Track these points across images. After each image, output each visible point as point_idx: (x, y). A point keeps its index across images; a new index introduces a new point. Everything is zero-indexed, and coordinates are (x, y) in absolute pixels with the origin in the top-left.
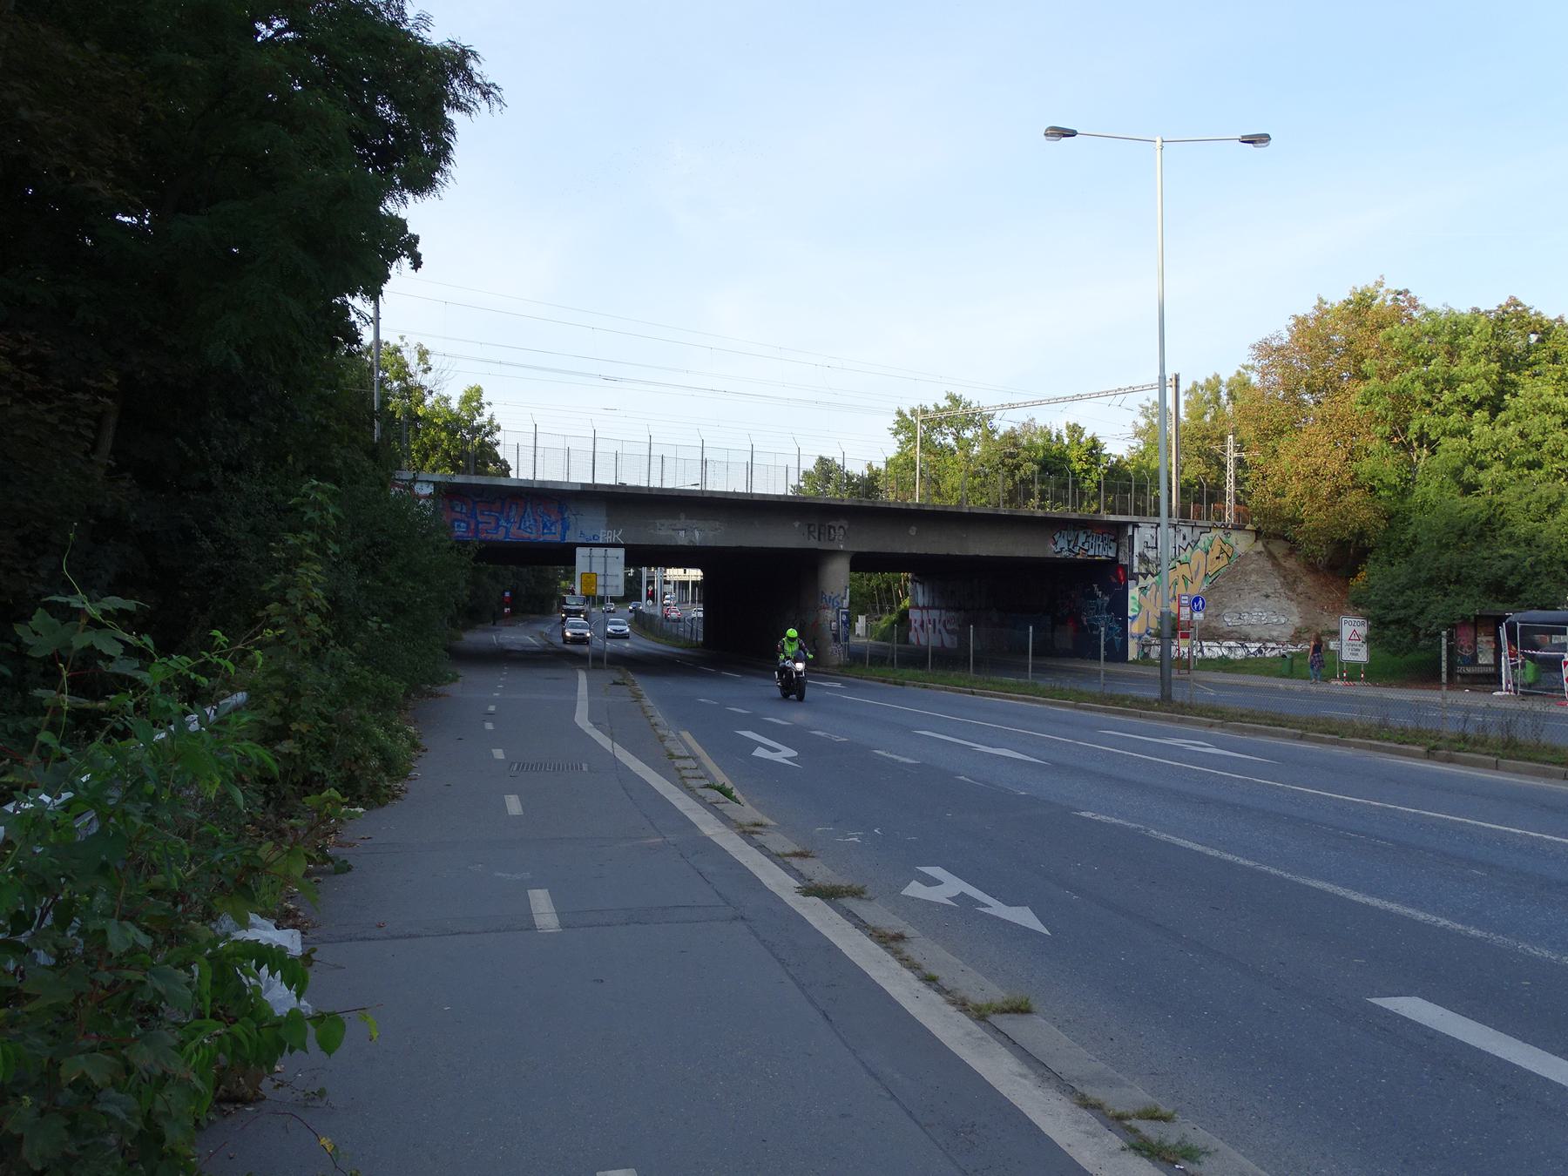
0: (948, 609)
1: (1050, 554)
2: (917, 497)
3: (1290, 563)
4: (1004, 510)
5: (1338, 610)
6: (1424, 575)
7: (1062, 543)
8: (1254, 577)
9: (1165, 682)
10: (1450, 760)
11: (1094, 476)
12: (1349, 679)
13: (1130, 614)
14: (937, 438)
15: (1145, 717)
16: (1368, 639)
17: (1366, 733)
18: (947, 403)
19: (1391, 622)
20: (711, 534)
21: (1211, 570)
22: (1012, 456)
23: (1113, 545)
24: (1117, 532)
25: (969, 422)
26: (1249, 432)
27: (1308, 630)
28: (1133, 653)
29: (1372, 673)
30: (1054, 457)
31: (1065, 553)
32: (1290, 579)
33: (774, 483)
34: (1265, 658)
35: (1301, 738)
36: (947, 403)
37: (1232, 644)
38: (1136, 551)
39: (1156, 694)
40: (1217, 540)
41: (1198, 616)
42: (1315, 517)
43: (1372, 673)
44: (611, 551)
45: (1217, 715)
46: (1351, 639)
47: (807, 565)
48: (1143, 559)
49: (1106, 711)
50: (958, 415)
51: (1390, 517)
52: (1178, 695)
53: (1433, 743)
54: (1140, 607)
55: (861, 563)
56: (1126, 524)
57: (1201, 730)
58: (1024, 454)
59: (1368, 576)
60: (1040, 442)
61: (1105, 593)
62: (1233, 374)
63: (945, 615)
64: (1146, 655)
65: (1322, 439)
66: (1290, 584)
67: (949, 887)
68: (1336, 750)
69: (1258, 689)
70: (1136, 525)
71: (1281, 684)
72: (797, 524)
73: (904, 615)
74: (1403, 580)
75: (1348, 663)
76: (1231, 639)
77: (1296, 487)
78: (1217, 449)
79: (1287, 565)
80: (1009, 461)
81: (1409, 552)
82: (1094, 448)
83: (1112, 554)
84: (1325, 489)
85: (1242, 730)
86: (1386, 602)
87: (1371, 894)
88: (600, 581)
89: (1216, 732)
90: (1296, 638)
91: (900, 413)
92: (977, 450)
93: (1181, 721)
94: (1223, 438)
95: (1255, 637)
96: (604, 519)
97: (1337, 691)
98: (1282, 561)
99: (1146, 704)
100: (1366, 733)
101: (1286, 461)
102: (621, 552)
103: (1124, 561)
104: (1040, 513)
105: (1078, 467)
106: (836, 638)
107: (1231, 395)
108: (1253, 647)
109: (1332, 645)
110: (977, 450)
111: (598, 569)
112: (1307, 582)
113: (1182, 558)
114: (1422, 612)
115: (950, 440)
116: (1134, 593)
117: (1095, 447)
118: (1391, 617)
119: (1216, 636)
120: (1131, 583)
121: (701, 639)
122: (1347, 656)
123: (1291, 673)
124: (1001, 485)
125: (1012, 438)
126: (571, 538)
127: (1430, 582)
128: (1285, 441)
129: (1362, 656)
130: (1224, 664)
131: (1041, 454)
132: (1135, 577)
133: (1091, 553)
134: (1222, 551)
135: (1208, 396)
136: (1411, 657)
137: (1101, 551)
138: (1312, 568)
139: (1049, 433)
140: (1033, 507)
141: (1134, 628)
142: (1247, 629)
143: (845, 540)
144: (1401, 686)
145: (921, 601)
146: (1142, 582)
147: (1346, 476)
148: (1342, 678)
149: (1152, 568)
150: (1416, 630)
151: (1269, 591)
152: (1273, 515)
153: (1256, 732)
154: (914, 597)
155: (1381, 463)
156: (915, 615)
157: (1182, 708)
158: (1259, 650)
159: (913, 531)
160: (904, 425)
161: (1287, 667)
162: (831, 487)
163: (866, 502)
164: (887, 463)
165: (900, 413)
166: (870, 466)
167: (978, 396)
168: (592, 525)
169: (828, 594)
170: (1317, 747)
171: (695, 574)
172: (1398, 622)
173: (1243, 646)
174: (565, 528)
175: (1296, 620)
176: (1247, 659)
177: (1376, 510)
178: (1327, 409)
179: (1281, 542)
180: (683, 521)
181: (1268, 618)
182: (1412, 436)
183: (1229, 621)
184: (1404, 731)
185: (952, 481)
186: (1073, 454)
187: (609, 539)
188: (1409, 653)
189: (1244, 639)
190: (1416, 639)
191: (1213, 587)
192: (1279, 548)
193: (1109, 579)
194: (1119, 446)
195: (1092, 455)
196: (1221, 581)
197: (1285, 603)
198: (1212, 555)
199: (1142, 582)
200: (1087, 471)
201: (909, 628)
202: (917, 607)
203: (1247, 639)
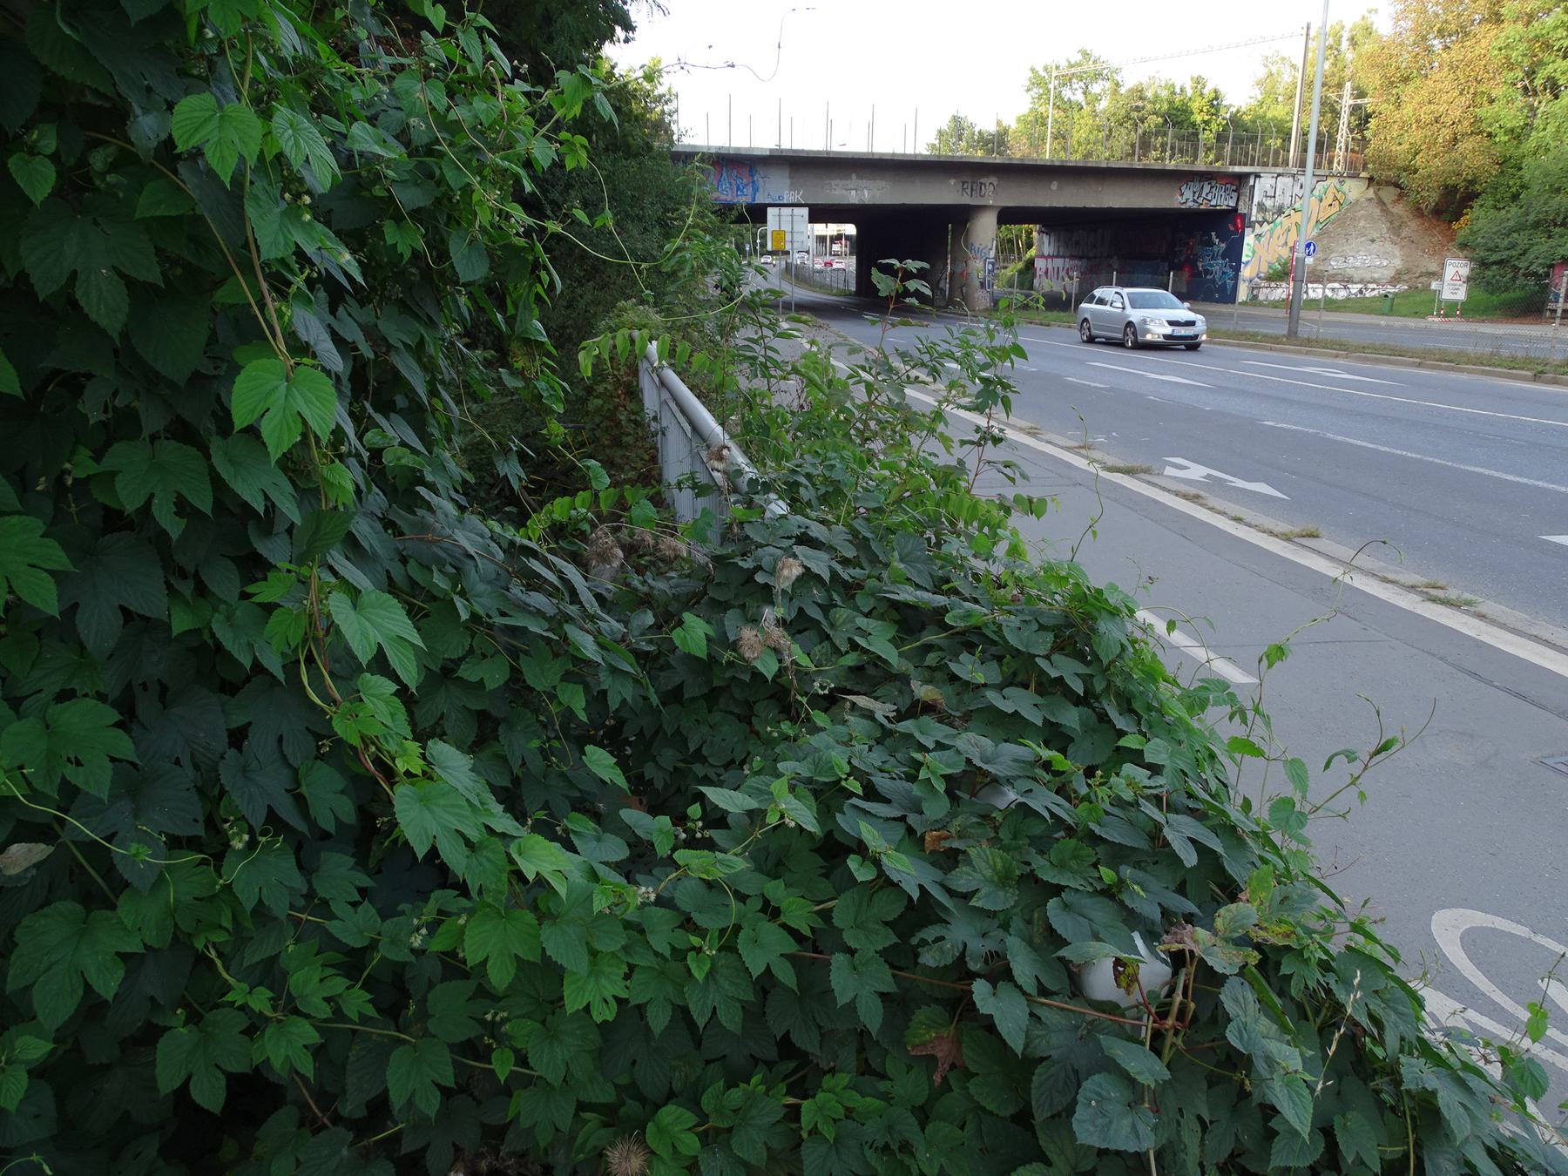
0: (1072, 257)
1: (1176, 206)
2: (1048, 153)
3: (1399, 209)
4: (1123, 164)
5: (1440, 253)
6: (1531, 218)
7: (1188, 194)
8: (1362, 223)
9: (1293, 320)
10: (1555, 382)
11: (1214, 127)
12: (1445, 316)
13: (1244, 259)
14: (1067, 93)
15: (1276, 350)
16: (1469, 279)
17: (1478, 361)
18: (1079, 57)
19: (1494, 263)
20: (878, 193)
22: (1138, 109)
23: (1235, 195)
24: (1239, 182)
25: (1098, 76)
26: (1372, 81)
27: (1408, 271)
28: (1243, 294)
29: (1468, 310)
30: (1177, 109)
31: (1190, 204)
32: (1397, 224)
33: (919, 143)
35: (1419, 365)
36: (1079, 57)
37: (1336, 285)
38: (1256, 200)
39: (1283, 330)
40: (1332, 189)
41: (1309, 260)
42: (1432, 165)
43: (1468, 310)
44: (796, 210)
45: (1339, 347)
46: (1454, 279)
47: (961, 216)
48: (1262, 208)
49: (1238, 345)
50: (1088, 71)
51: (1503, 162)
52: (1304, 331)
53: (1540, 368)
54: (1254, 252)
55: (1008, 216)
56: (1248, 175)
57: (1329, 360)
58: (1149, 106)
59: (1478, 219)
60: (1164, 94)
61: (1222, 241)
62: (1358, 19)
63: (1068, 263)
64: (1255, 297)
65: (1446, 86)
66: (1396, 228)
67: (1197, 472)
68: (1453, 375)
69: (1362, 326)
70: (1257, 176)
71: (1383, 321)
72: (952, 182)
73: (1030, 264)
74: (1511, 223)
75: (1447, 301)
77: (1416, 136)
78: (1333, 97)
79: (1395, 210)
80: (1134, 115)
81: (1515, 197)
82: (1215, 103)
83: (1232, 204)
84: (1446, 133)
85: (1366, 360)
86: (1491, 245)
87: (1520, 475)
88: (788, 237)
89: (1341, 361)
90: (1394, 281)
91: (1033, 70)
92: (1103, 105)
93: (1307, 353)
94: (1340, 86)
96: (788, 181)
97: (1435, 326)
98: (1389, 206)
99: (1276, 339)
100: (1478, 361)
101: (1408, 110)
102: (805, 211)
103: (1242, 209)
104: (1157, 166)
105: (1198, 118)
106: (982, 285)
107: (1353, 42)
108: (1354, 288)
109: (1434, 285)
110: (1103, 105)
111: (786, 227)
112: (1414, 224)
113: (1297, 206)
114: (1524, 253)
115: (1079, 97)
116: (1249, 239)
117: (1216, 98)
118: (1494, 257)
119: (1318, 277)
120: (1247, 231)
121: (853, 289)
122: (1447, 295)
123: (1391, 312)
124: (1124, 137)
125: (1139, 93)
126: (761, 199)
127: (1536, 224)
128: (1410, 88)
129: (1461, 295)
130: (1330, 305)
131: (1166, 106)
132: (1252, 225)
134: (1335, 199)
135: (1330, 41)
136: (1505, 296)
137: (1220, 200)
138: (1418, 212)
139: (1173, 86)
140: (1151, 161)
141: (1246, 272)
143: (996, 195)
144: (1492, 321)
145: (1047, 250)
147: (1466, 123)
148: (1439, 315)
149: (1269, 217)
150: (1516, 269)
151: (1376, 235)
152: (1385, 161)
153: (1378, 361)
154: (1041, 246)
155: (1507, 111)
156: (1040, 264)
157: (1308, 342)
158: (1361, 291)
159: (1054, 186)
160: (1038, 81)
161: (1387, 306)
162: (963, 144)
163: (996, 159)
164: (1019, 120)
165: (1033, 70)
166: (999, 123)
167: (1109, 53)
168: (774, 187)
169: (977, 246)
170: (1434, 373)
171: (850, 229)
172: (1500, 262)
174: (756, 190)
175: (1398, 263)
176: (1348, 299)
177: (1491, 156)
178: (1456, 54)
179: (1392, 189)
180: (854, 181)
181: (1372, 260)
182: (1538, 82)
183: (1335, 264)
184: (1514, 359)
185: (1079, 134)
186: (1195, 106)
187: (792, 200)
188: (1513, 289)
189: (1347, 281)
190: (1514, 279)
191: (1323, 233)
192: (1389, 194)
193: (1226, 226)
194: (1240, 97)
195: (1212, 106)
196: (1330, 227)
197: (1388, 247)
198: (1326, 202)
199: (1258, 229)
200: (1206, 123)
201: (1034, 275)
202: (1043, 256)
203: (1350, 280)
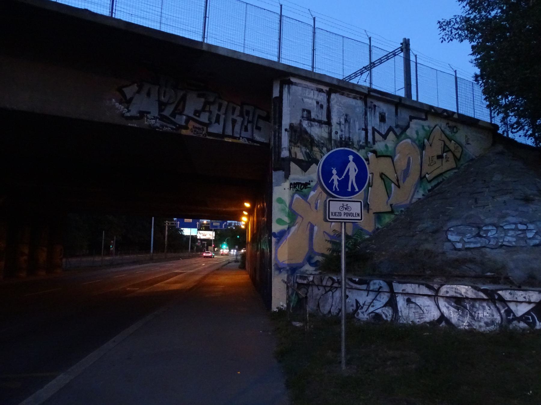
21: (431, 172)
31: (151, 121)
34: (180, 135)
37: (464, 290)
38: (286, 122)
40: (437, 132)
48: (299, 135)
54: (293, 215)
76: (460, 279)
95: (517, 274)
113: (380, 146)
120: (277, 175)
132: (284, 166)
133: (216, 129)
134: (445, 149)
137: (228, 126)
142: (499, 256)
146: (297, 174)
173: (493, 298)
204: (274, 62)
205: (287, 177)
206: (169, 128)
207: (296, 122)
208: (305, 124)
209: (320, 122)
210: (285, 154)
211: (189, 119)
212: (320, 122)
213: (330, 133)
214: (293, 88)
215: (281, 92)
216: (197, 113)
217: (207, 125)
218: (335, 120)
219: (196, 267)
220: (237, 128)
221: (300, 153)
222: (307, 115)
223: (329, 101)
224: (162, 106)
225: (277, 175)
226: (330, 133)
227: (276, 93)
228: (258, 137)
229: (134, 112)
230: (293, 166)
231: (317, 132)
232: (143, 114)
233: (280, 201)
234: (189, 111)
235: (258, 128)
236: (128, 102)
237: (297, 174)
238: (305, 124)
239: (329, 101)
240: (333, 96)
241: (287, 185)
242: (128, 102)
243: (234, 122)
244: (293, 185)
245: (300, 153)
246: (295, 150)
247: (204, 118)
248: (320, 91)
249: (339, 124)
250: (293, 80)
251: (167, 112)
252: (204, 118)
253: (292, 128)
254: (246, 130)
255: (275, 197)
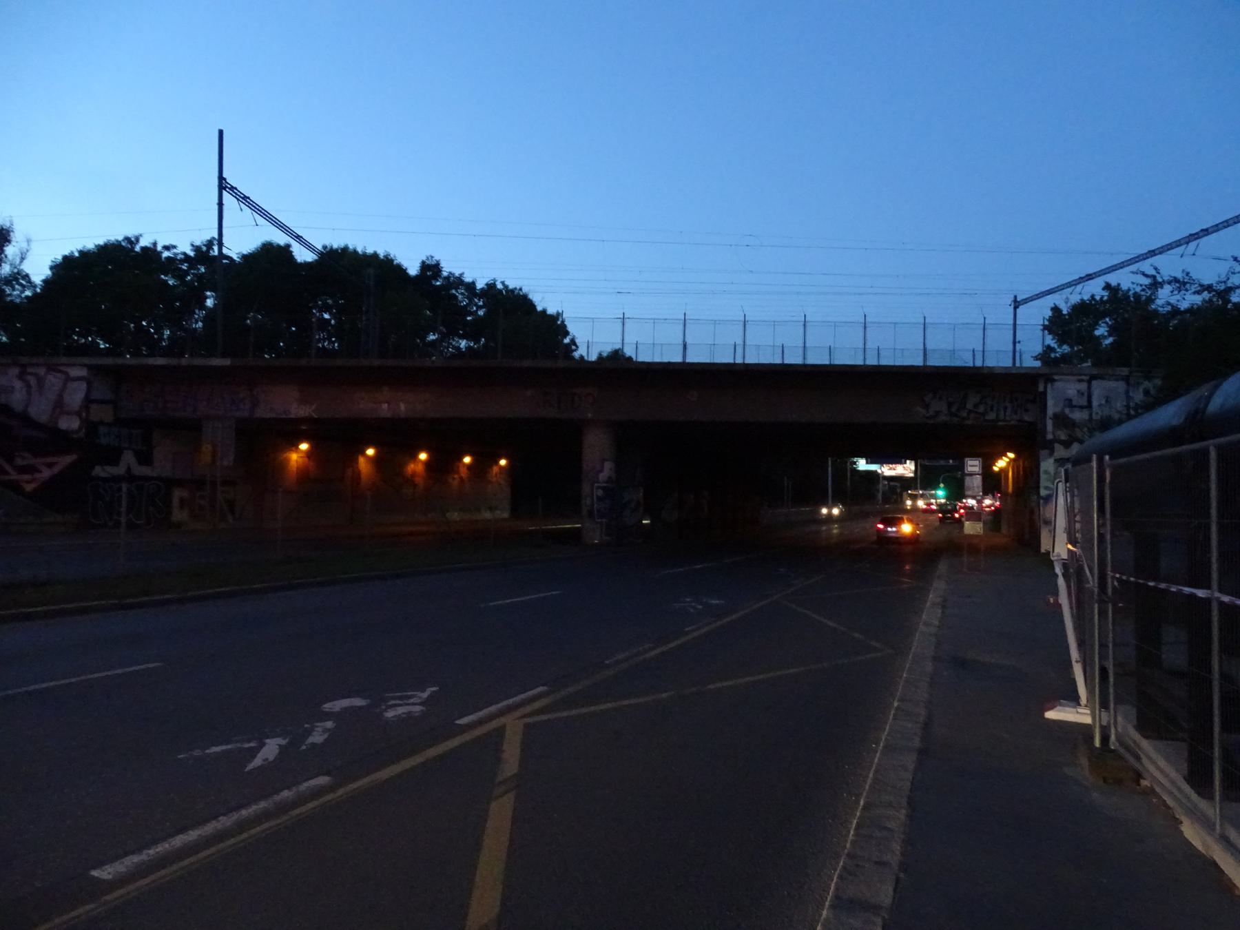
31: (943, 418)
38: (1050, 411)
132: (1049, 446)
133: (991, 416)
146: (1060, 452)
204: (1039, 546)
205: (1051, 454)
206: (955, 420)
207: (1058, 410)
208: (1067, 411)
209: (1082, 407)
210: (1050, 437)
211: (970, 411)
212: (1082, 407)
213: (1091, 415)
214: (1057, 384)
215: (1045, 388)
216: (976, 406)
217: (983, 414)
218: (1095, 403)
219: (1173, 782)
220: (1009, 411)
221: (1063, 436)
222: (1069, 403)
223: (1089, 388)
224: (950, 405)
225: (1044, 453)
226: (1091, 415)
227: (1041, 388)
228: (1026, 418)
229: (931, 412)
230: (1057, 446)
231: (1077, 416)
232: (937, 413)
233: (1046, 472)
234: (969, 406)
235: (1026, 410)
236: (927, 406)
237: (1060, 452)
238: (1067, 411)
239: (1089, 388)
240: (1094, 382)
241: (1051, 461)
242: (927, 406)
243: (1006, 408)
244: (1057, 461)
245: (1063, 436)
246: (1059, 432)
247: (981, 409)
248: (1081, 381)
249: (1100, 405)
250: (1056, 377)
251: (954, 409)
252: (981, 409)
253: (1056, 417)
254: (1016, 413)
255: (1042, 470)
